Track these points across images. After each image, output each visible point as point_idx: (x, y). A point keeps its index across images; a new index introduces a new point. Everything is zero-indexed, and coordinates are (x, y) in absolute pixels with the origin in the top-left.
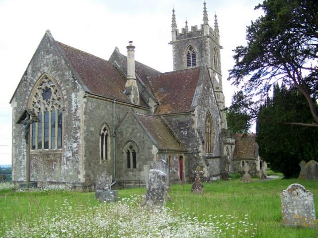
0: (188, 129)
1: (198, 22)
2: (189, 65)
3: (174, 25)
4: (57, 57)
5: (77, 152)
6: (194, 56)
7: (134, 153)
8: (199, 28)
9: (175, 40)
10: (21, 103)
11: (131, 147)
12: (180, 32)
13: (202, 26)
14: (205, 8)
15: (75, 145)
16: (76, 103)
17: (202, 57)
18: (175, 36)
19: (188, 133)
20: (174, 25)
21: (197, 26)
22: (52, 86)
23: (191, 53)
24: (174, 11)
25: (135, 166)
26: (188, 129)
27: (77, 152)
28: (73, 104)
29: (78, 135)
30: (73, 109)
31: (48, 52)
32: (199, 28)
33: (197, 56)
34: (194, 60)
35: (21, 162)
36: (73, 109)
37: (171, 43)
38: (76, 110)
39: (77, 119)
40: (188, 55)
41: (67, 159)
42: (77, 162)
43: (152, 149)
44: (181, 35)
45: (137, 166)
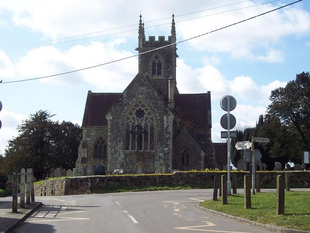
0: (205, 140)
1: (167, 34)
2: (154, 73)
3: (141, 31)
4: (150, 90)
5: (168, 154)
6: (160, 65)
7: (187, 155)
8: (166, 39)
9: (141, 47)
10: (116, 117)
11: (185, 151)
12: (147, 39)
13: (169, 37)
14: (173, 20)
15: (166, 149)
16: (167, 122)
17: (168, 68)
18: (142, 43)
19: (205, 143)
20: (141, 31)
21: (164, 37)
22: (145, 109)
23: (157, 62)
24: (141, 16)
25: (188, 164)
26: (205, 140)
27: (168, 154)
28: (165, 123)
29: (169, 143)
30: (165, 126)
31: (142, 85)
32: (166, 39)
33: (163, 66)
34: (159, 70)
35: (117, 158)
36: (165, 126)
37: (137, 49)
38: (167, 127)
39: (168, 133)
40: (154, 63)
41: (160, 158)
42: (168, 159)
43: (201, 153)
44: (147, 42)
45: (190, 163)
